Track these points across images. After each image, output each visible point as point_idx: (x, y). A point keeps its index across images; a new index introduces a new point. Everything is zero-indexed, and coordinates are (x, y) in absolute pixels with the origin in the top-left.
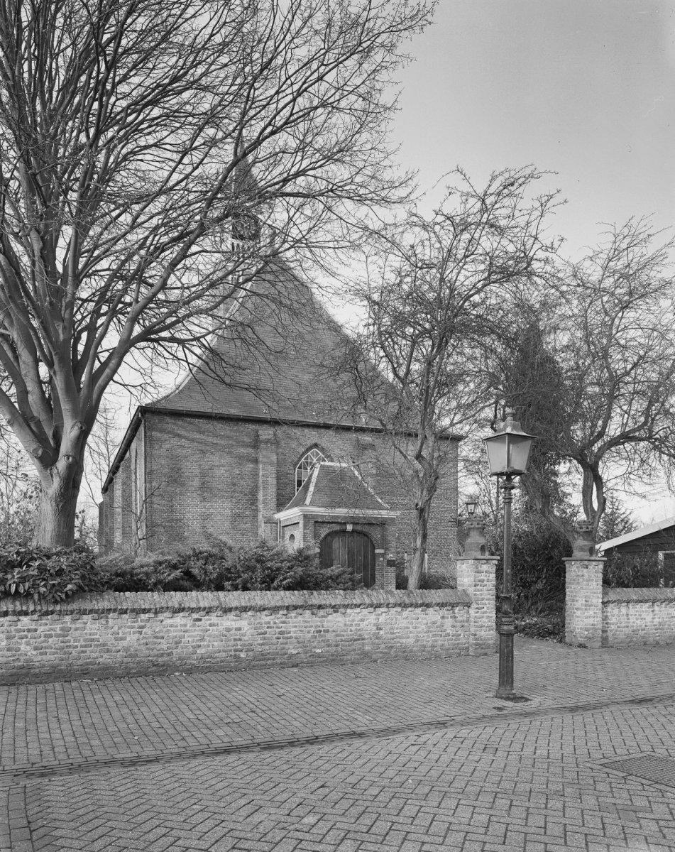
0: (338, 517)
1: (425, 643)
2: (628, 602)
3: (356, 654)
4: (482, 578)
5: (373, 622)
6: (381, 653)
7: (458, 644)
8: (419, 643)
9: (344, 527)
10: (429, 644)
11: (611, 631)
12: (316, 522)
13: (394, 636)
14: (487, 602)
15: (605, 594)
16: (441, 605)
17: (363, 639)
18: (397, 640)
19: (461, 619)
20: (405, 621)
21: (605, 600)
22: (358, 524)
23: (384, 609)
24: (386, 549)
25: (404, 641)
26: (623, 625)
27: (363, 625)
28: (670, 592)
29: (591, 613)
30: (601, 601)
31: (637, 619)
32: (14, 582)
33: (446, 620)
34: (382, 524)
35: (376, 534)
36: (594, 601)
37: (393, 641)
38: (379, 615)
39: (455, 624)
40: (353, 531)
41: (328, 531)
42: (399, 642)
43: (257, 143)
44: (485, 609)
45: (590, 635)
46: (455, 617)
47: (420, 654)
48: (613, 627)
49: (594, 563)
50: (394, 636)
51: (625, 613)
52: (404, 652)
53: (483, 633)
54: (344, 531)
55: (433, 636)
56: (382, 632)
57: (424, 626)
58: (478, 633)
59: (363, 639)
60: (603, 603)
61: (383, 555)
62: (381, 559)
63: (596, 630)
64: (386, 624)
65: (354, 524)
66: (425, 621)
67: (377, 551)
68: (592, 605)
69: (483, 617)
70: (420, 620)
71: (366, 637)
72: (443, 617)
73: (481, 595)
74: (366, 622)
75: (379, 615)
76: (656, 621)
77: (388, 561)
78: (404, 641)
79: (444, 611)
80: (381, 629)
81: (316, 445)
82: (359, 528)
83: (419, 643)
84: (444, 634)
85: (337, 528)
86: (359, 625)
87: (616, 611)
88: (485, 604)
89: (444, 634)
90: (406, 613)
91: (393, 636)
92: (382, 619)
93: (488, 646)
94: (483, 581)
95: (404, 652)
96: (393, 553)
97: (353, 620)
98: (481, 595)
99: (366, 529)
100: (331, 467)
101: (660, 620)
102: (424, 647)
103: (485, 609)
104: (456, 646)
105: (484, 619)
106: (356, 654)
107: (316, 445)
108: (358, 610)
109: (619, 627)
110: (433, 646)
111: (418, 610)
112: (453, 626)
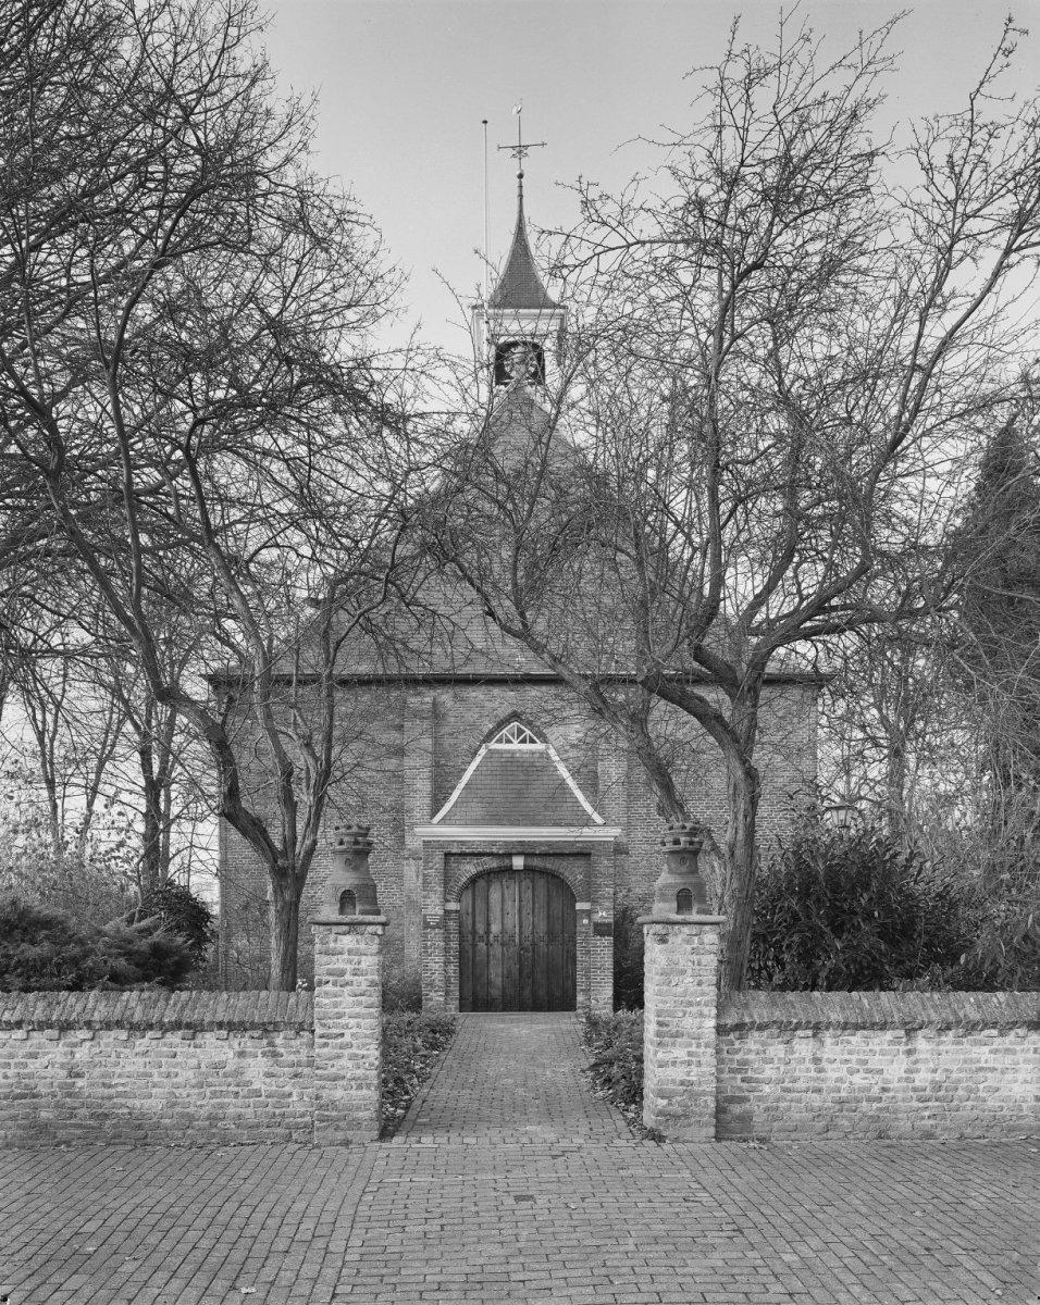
0: (493, 843)
1: (192, 1110)
2: (817, 1028)
3: (19, 1127)
4: (341, 966)
5: (60, 1059)
6: (80, 1126)
7: (283, 1115)
8: (178, 1109)
9: (507, 861)
10: (203, 1112)
11: (760, 1099)
12: (448, 855)
13: (112, 1091)
14: (352, 1022)
15: (721, 1009)
16: (232, 1027)
17: (34, 1096)
18: (123, 1101)
19: (292, 1058)
20: (141, 1060)
21: (730, 1021)
22: (534, 855)
23: (84, 1034)
24: (594, 902)
25: (137, 1103)
26: (801, 1085)
27: (34, 1066)
28: (1031, 1002)
29: (680, 1053)
30: (712, 1023)
31: (851, 1072)
32: (43, 976)
33: (250, 1060)
34: (583, 853)
35: (574, 873)
36: (689, 1023)
37: (108, 1103)
38: (75, 1045)
39: (276, 1070)
40: (527, 869)
41: (474, 871)
42: (122, 1106)
43: (884, 278)
44: (347, 1038)
45: (676, 1109)
46: (275, 1055)
47: (179, 1134)
48: (767, 1089)
49: (686, 929)
50: (112, 1091)
51: (809, 1056)
52: (139, 1127)
53: (339, 1094)
54: (509, 870)
55: (214, 1094)
56: (80, 1083)
57: (190, 1074)
58: (324, 1093)
59: (34, 1096)
60: (721, 1030)
61: (588, 914)
62: (585, 921)
63: (694, 1096)
64: (92, 1064)
65: (526, 855)
66: (194, 1062)
67: (579, 906)
68: (678, 1035)
69: (339, 1057)
70: (179, 1059)
71: (43, 1090)
72: (242, 1054)
73: (336, 1005)
74: (45, 1060)
75: (75, 1045)
76: (923, 1078)
77: (597, 925)
78: (137, 1103)
79: (245, 1041)
80: (78, 1075)
81: (515, 716)
82: (536, 862)
83: (178, 1109)
84: (243, 1091)
85: (493, 864)
86: (26, 1065)
87: (777, 1050)
88: (347, 1026)
89: (243, 1091)
90: (143, 1042)
91: (107, 1092)
92: (82, 1054)
93: (356, 1124)
94: (342, 973)
95: (139, 1127)
96: (608, 909)
97: (11, 1056)
98: (336, 1005)
99: (549, 864)
100: (508, 751)
101: (938, 1077)
102: (191, 1118)
103: (347, 1038)
104: (274, 1121)
105: (344, 1062)
106: (19, 1127)
107: (515, 716)
108: (20, 1034)
109: (788, 1090)
110: (213, 1118)
111: (174, 1038)
112: (269, 1075)
